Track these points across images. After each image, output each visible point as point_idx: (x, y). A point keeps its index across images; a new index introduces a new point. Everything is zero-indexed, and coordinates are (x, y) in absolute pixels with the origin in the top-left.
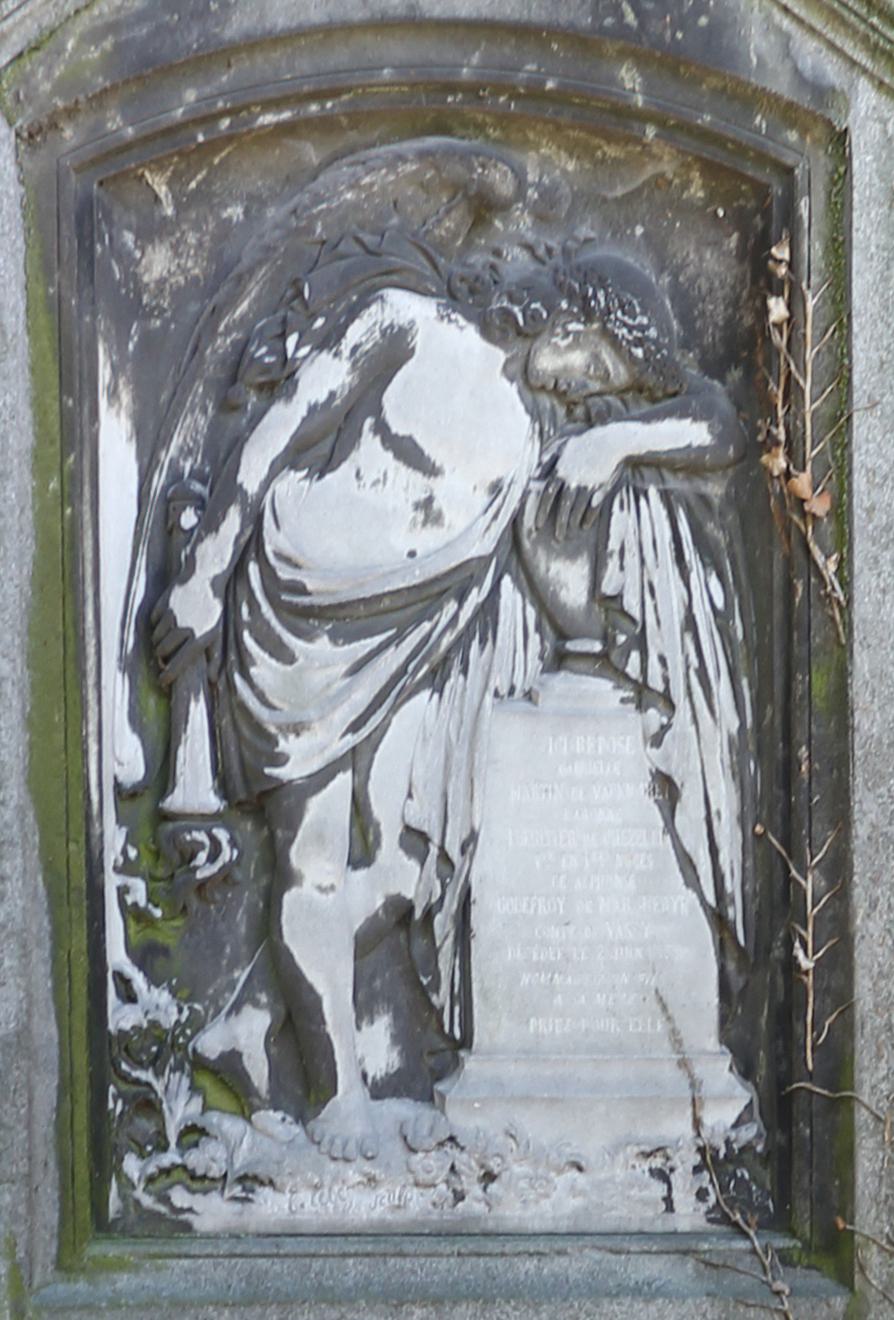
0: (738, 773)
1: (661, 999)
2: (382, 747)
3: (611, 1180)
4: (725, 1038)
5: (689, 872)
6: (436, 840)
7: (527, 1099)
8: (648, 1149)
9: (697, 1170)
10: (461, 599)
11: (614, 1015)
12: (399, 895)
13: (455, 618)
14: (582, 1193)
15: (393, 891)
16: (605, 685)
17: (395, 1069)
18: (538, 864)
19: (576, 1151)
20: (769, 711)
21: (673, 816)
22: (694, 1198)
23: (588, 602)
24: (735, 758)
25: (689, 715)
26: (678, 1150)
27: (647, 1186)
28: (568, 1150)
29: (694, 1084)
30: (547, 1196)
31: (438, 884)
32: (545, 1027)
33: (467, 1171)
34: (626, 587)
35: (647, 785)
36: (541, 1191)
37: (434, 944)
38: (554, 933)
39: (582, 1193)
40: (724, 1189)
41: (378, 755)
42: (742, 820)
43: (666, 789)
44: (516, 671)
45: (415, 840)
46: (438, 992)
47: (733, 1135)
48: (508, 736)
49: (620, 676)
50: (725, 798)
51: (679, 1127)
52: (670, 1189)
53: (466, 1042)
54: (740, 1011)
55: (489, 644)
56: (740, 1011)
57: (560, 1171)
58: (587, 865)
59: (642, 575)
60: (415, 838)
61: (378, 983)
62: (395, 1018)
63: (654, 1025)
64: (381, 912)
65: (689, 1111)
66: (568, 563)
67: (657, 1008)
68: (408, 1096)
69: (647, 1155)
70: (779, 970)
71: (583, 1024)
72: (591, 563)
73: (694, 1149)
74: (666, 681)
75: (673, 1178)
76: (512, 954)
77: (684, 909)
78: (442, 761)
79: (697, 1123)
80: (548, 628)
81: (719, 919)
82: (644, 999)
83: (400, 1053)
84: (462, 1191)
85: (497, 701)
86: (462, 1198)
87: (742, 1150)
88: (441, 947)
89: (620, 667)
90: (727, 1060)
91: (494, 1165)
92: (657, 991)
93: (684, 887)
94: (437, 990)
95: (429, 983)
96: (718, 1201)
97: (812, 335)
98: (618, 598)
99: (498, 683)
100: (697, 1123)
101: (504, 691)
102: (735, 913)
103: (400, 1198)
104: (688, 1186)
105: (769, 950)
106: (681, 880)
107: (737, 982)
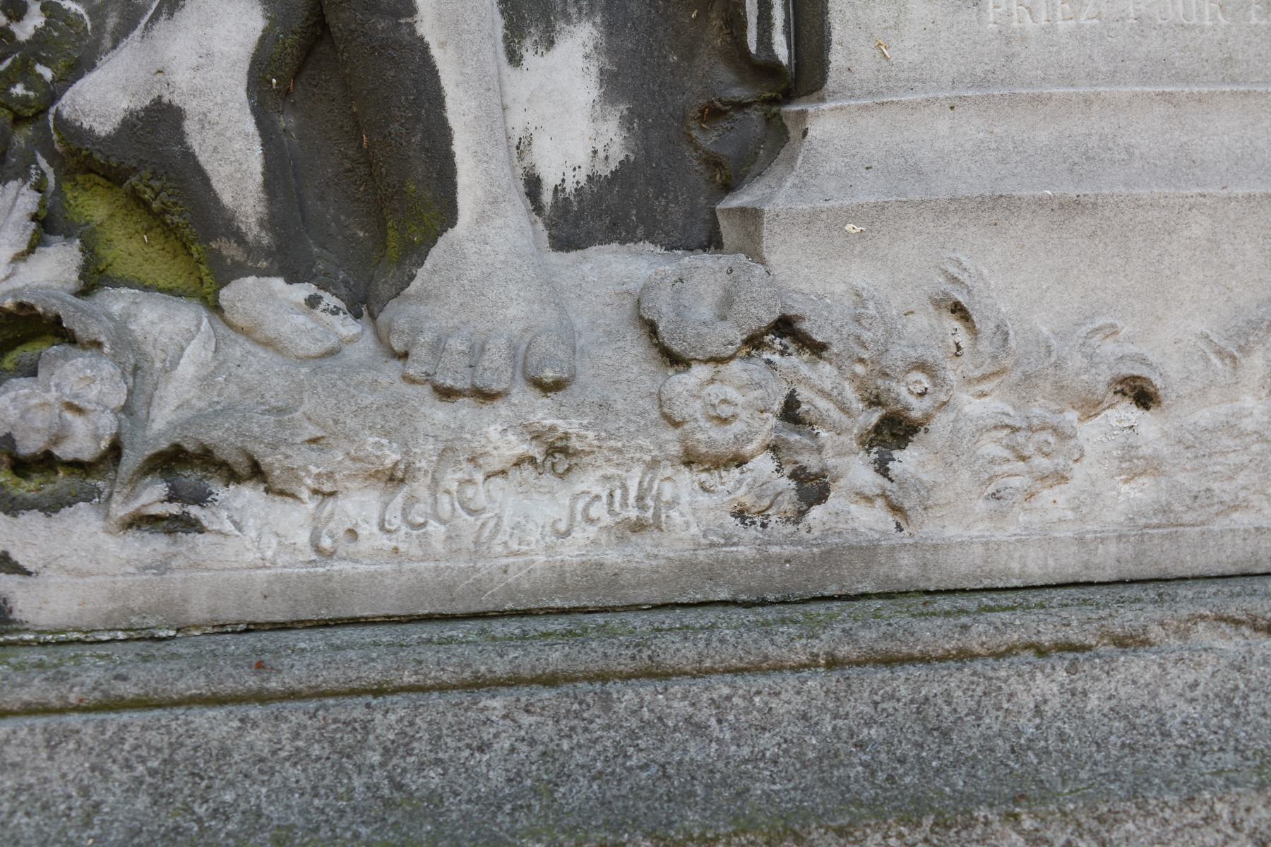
3: (1229, 427)
7: (996, 206)
14: (1153, 467)
17: (613, 166)
19: (1131, 349)
28: (1109, 348)
30: (1061, 477)
36: (1041, 462)
39: (1153, 467)
57: (1091, 407)
62: (611, 29)
68: (649, 237)
83: (626, 122)
84: (821, 475)
91: (907, 393)
103: (640, 498)
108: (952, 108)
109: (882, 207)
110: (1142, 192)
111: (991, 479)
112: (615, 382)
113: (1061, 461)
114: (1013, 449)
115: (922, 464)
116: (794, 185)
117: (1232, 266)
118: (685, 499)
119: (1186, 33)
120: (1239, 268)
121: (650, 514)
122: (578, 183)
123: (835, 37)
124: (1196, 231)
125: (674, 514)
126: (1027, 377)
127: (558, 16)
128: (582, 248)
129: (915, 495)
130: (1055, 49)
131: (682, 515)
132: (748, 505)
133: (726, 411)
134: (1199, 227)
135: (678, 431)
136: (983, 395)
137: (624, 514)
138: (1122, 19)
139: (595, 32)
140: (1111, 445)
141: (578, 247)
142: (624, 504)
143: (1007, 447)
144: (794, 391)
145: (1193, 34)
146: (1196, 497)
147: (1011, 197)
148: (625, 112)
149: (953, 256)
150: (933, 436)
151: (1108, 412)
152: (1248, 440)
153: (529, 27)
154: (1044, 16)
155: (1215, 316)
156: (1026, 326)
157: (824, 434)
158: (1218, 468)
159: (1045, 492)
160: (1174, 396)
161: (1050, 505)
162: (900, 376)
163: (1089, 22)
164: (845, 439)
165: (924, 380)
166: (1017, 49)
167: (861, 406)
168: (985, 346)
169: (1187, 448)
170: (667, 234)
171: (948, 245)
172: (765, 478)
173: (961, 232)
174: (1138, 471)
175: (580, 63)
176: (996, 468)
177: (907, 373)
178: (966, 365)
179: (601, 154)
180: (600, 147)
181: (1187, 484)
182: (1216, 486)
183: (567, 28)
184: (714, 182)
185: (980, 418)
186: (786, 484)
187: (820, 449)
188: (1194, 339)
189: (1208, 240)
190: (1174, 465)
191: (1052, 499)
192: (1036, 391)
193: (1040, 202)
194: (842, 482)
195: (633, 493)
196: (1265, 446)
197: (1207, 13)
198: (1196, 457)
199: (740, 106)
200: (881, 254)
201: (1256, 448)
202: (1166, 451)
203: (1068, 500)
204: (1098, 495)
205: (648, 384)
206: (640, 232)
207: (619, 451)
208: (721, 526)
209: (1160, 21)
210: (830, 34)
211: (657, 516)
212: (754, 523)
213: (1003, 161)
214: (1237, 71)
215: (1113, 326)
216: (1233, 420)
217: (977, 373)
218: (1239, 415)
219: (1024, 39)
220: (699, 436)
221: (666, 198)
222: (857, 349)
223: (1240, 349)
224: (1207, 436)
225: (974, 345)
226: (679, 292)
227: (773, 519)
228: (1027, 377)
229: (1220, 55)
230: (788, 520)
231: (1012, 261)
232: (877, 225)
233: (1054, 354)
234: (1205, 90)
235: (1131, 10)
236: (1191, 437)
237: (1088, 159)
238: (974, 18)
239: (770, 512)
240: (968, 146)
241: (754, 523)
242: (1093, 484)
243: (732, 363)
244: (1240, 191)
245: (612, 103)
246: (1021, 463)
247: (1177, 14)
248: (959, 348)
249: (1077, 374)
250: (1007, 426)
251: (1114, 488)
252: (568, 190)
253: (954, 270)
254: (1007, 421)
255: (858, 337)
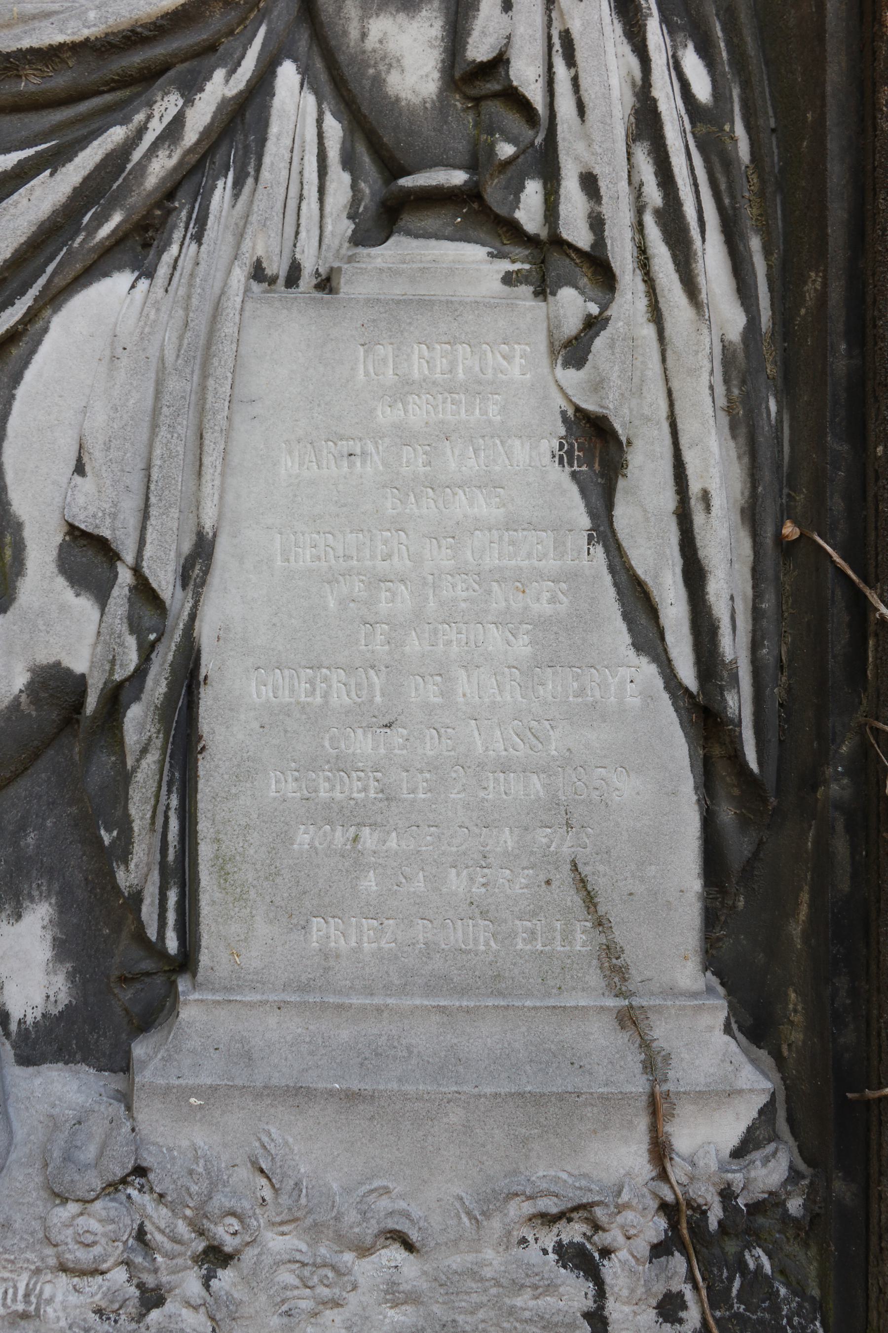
0: (742, 420)
1: (582, 882)
2: (29, 375)
3: (473, 1274)
4: (712, 959)
5: (643, 620)
6: (129, 557)
7: (298, 1095)
8: (552, 1206)
9: (659, 1250)
10: (191, 88)
11: (484, 914)
12: (58, 664)
13: (178, 122)
14: (413, 1298)
15: (44, 657)
16: (473, 253)
17: (60, 1007)
18: (332, 604)
19: (402, 1205)
20: (813, 285)
21: (610, 505)
22: (652, 1314)
23: (441, 91)
24: (736, 391)
25: (642, 303)
26: (621, 1209)
27: (551, 1288)
28: (384, 1203)
29: (653, 1063)
30: (336, 1304)
31: (131, 642)
32: (345, 937)
33: (168, 1245)
34: (517, 42)
35: (556, 444)
36: (324, 1292)
37: (124, 763)
38: (363, 745)
39: (413, 1298)
40: (717, 1297)
41: (21, 392)
42: (751, 515)
43: (595, 445)
44: (303, 235)
45: (88, 555)
46: (126, 863)
47: (737, 1179)
48: (280, 344)
49: (505, 231)
50: (717, 466)
51: (623, 1158)
52: (601, 1294)
53: (186, 962)
54: (741, 904)
55: (250, 181)
56: (741, 904)
57: (364, 1251)
58: (432, 605)
59: (549, 24)
60: (87, 556)
61: (31, 839)
62: (62, 908)
63: (567, 937)
64: (23, 698)
65: (642, 1123)
66: (401, 17)
67: (574, 899)
68: (84, 1060)
69: (548, 1219)
70: (840, 826)
71: (421, 931)
72: (447, 15)
73: (654, 1205)
74: (597, 223)
75: (611, 1270)
76: (278, 786)
77: (634, 701)
78: (149, 403)
79: (660, 1152)
80: (366, 160)
81: (704, 718)
82: (548, 882)
83: (71, 976)
84: (158, 1288)
85: (256, 287)
86: (159, 1302)
87: (756, 1208)
88: (135, 769)
89: (502, 211)
90: (717, 1011)
91: (225, 1234)
92: (575, 867)
93: (631, 652)
94: (125, 857)
95: (113, 842)
96: (704, 1322)
97: (732, 103)
98: (499, 62)
99: (260, 252)
100: (660, 1152)
101: (277, 267)
102: (740, 703)
103: (27, 1295)
104: (640, 1291)
105: (812, 781)
106: (626, 638)
107: (739, 847)
108: (279, 1008)
109: (214, 1089)
110: (409, 1088)
111: (283, 1302)
112: (20, 1204)
113: (337, 1291)
114: (301, 1279)
115: (234, 1285)
116: (163, 1057)
117: (483, 1146)
118: (59, 1298)
119: (464, 956)
120: (489, 1147)
121: (32, 1308)
122: (35, 1018)
123: (204, 943)
124: (453, 1119)
125: (49, 1310)
126: (316, 1224)
127: (25, 897)
128: (38, 1065)
129: (224, 1309)
130: (361, 965)
131: (55, 1311)
132: (103, 1307)
133: (90, 1239)
134: (455, 1116)
135: (55, 1249)
136: (283, 1234)
137: (14, 1308)
138: (414, 944)
139: (51, 910)
140: (379, 1280)
141: (35, 1064)
142: (14, 1300)
143: (298, 1277)
144: (143, 1222)
145: (469, 957)
146: (444, 1326)
147: (309, 1088)
148: (70, 969)
149: (266, 1127)
150: (243, 1265)
151: (383, 1251)
152: (487, 1284)
153: (4, 904)
154: (354, 939)
155: (470, 1182)
156: (321, 1182)
157: (159, 1259)
158: (463, 1304)
159: (328, 1312)
160: (432, 1244)
161: (329, 1323)
162: (218, 1220)
163: (388, 945)
164: (180, 1261)
165: (235, 1224)
166: (332, 963)
167: (193, 1235)
168: (284, 1200)
169: (441, 1285)
170: (98, 1059)
171: (262, 1119)
172: (117, 1287)
173: (272, 1110)
174: (399, 1301)
175: (40, 932)
176: (288, 1293)
177: (224, 1217)
178: (271, 1212)
179: (52, 999)
180: (51, 994)
181: (439, 1314)
182: (460, 1318)
183: (31, 906)
184: (133, 1024)
185: (279, 1253)
186: (133, 1291)
187: (156, 1271)
188: (452, 1200)
189: (463, 1126)
190: (430, 1298)
191: (331, 1318)
192: (322, 1236)
193: (331, 1093)
194: (177, 1291)
195: (21, 1292)
196: (501, 1290)
197: (482, 940)
198: (447, 1293)
199: (148, 974)
200: (215, 1121)
201: (494, 1291)
202: (425, 1286)
203: (343, 1321)
204: (367, 1318)
205: (40, 1209)
206: (78, 1057)
207: (12, 1262)
208: (84, 1320)
209: (443, 946)
210: (200, 940)
211: (37, 1309)
212: (109, 1319)
213: (312, 1053)
214: (504, 985)
215: (386, 1188)
216: (475, 1268)
217: (278, 1219)
218: (482, 1264)
219: (338, 956)
220: (68, 1256)
221: (98, 1033)
222: (187, 1198)
223: (483, 1213)
224: (456, 1278)
225: (276, 1198)
226: (74, 1134)
227: (123, 1317)
228: (316, 1224)
229: (490, 973)
230: (133, 1319)
231: (311, 1133)
232: (212, 1101)
233: (335, 1210)
234: (472, 1004)
235: (421, 937)
236: (444, 1277)
237: (376, 1055)
238: (302, 939)
239: (121, 1312)
240: (289, 1038)
241: (109, 1319)
242: (364, 1309)
243: (96, 1202)
244: (488, 1090)
245: (61, 962)
246: (308, 1290)
247: (457, 941)
248: (264, 1200)
249: (351, 1227)
250: (297, 1262)
251: (381, 1314)
252: (28, 1023)
253: (265, 1139)
254: (298, 1257)
255: (188, 1189)
